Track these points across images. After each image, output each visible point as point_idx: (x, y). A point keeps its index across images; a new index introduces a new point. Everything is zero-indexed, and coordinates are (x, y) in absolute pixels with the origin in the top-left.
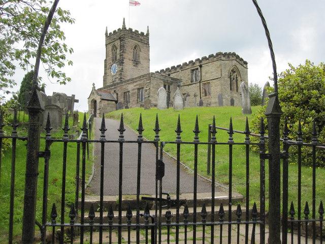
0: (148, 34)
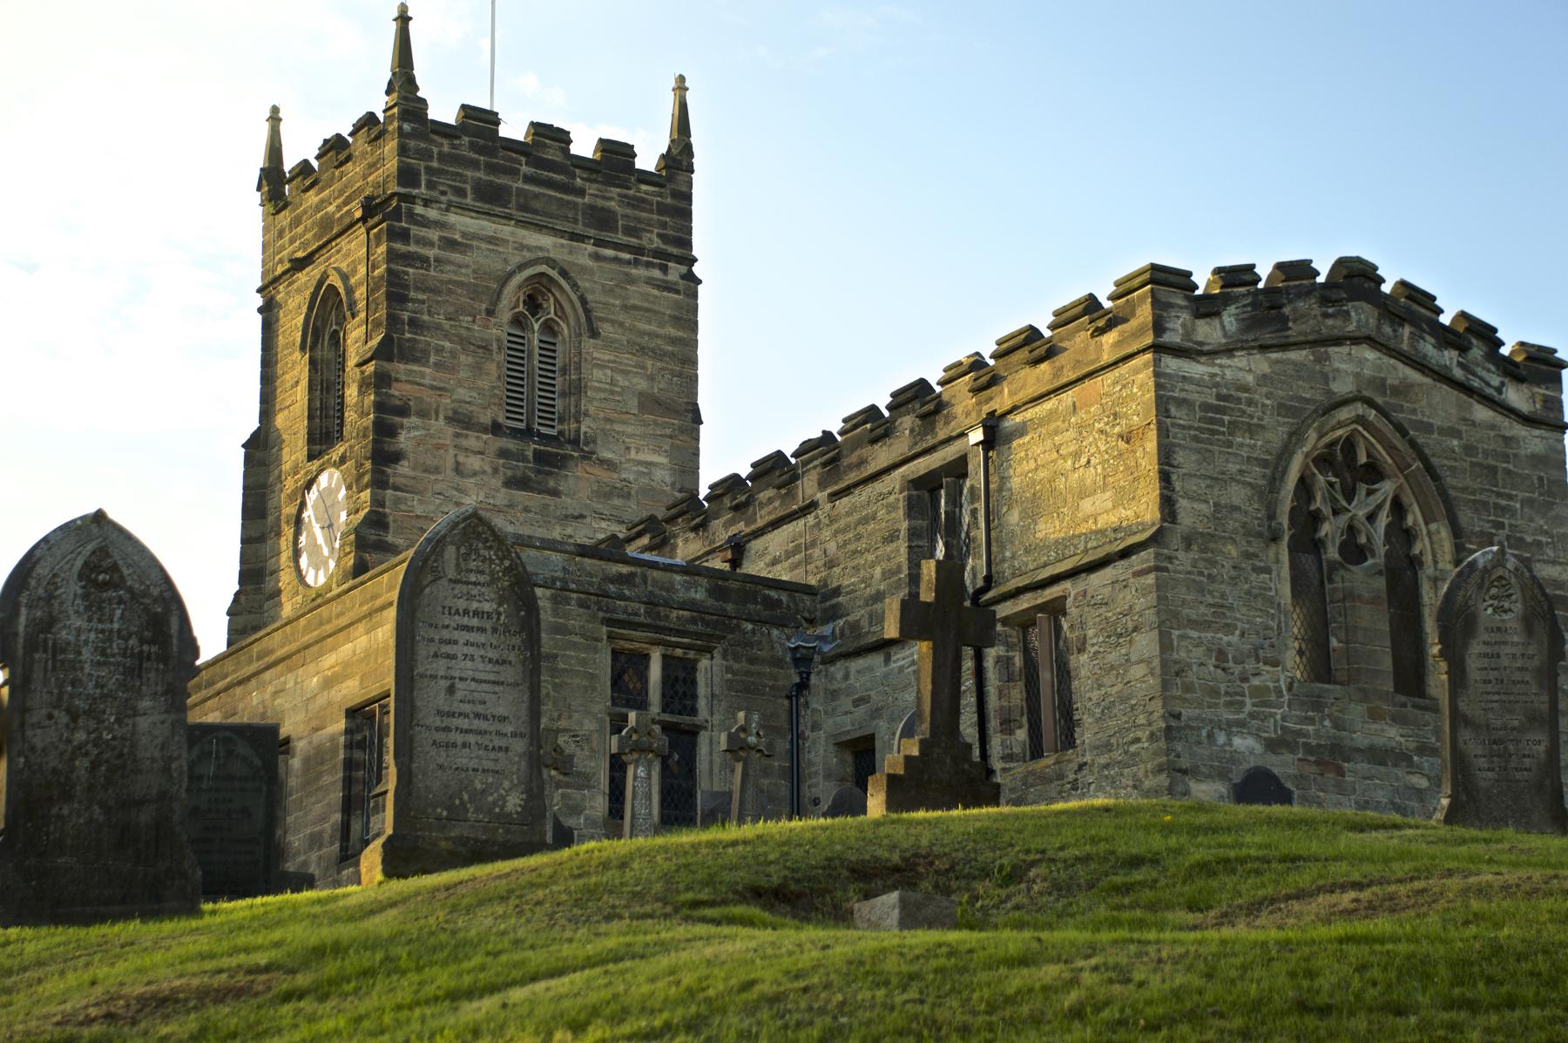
0: (679, 159)
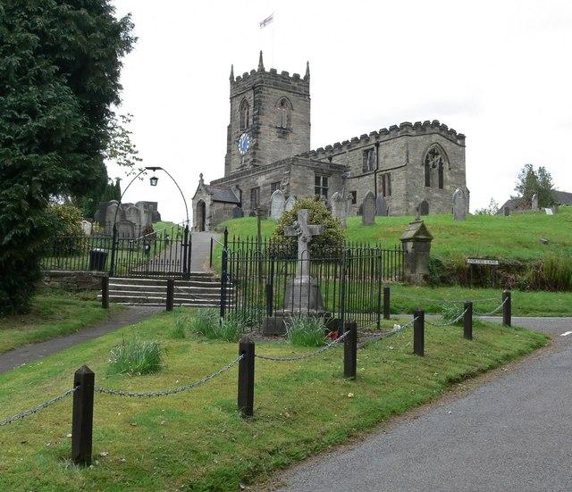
0: (307, 77)
